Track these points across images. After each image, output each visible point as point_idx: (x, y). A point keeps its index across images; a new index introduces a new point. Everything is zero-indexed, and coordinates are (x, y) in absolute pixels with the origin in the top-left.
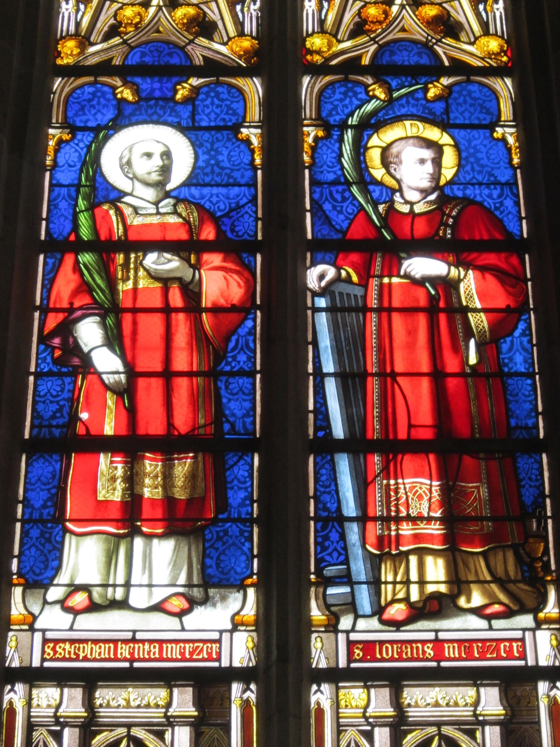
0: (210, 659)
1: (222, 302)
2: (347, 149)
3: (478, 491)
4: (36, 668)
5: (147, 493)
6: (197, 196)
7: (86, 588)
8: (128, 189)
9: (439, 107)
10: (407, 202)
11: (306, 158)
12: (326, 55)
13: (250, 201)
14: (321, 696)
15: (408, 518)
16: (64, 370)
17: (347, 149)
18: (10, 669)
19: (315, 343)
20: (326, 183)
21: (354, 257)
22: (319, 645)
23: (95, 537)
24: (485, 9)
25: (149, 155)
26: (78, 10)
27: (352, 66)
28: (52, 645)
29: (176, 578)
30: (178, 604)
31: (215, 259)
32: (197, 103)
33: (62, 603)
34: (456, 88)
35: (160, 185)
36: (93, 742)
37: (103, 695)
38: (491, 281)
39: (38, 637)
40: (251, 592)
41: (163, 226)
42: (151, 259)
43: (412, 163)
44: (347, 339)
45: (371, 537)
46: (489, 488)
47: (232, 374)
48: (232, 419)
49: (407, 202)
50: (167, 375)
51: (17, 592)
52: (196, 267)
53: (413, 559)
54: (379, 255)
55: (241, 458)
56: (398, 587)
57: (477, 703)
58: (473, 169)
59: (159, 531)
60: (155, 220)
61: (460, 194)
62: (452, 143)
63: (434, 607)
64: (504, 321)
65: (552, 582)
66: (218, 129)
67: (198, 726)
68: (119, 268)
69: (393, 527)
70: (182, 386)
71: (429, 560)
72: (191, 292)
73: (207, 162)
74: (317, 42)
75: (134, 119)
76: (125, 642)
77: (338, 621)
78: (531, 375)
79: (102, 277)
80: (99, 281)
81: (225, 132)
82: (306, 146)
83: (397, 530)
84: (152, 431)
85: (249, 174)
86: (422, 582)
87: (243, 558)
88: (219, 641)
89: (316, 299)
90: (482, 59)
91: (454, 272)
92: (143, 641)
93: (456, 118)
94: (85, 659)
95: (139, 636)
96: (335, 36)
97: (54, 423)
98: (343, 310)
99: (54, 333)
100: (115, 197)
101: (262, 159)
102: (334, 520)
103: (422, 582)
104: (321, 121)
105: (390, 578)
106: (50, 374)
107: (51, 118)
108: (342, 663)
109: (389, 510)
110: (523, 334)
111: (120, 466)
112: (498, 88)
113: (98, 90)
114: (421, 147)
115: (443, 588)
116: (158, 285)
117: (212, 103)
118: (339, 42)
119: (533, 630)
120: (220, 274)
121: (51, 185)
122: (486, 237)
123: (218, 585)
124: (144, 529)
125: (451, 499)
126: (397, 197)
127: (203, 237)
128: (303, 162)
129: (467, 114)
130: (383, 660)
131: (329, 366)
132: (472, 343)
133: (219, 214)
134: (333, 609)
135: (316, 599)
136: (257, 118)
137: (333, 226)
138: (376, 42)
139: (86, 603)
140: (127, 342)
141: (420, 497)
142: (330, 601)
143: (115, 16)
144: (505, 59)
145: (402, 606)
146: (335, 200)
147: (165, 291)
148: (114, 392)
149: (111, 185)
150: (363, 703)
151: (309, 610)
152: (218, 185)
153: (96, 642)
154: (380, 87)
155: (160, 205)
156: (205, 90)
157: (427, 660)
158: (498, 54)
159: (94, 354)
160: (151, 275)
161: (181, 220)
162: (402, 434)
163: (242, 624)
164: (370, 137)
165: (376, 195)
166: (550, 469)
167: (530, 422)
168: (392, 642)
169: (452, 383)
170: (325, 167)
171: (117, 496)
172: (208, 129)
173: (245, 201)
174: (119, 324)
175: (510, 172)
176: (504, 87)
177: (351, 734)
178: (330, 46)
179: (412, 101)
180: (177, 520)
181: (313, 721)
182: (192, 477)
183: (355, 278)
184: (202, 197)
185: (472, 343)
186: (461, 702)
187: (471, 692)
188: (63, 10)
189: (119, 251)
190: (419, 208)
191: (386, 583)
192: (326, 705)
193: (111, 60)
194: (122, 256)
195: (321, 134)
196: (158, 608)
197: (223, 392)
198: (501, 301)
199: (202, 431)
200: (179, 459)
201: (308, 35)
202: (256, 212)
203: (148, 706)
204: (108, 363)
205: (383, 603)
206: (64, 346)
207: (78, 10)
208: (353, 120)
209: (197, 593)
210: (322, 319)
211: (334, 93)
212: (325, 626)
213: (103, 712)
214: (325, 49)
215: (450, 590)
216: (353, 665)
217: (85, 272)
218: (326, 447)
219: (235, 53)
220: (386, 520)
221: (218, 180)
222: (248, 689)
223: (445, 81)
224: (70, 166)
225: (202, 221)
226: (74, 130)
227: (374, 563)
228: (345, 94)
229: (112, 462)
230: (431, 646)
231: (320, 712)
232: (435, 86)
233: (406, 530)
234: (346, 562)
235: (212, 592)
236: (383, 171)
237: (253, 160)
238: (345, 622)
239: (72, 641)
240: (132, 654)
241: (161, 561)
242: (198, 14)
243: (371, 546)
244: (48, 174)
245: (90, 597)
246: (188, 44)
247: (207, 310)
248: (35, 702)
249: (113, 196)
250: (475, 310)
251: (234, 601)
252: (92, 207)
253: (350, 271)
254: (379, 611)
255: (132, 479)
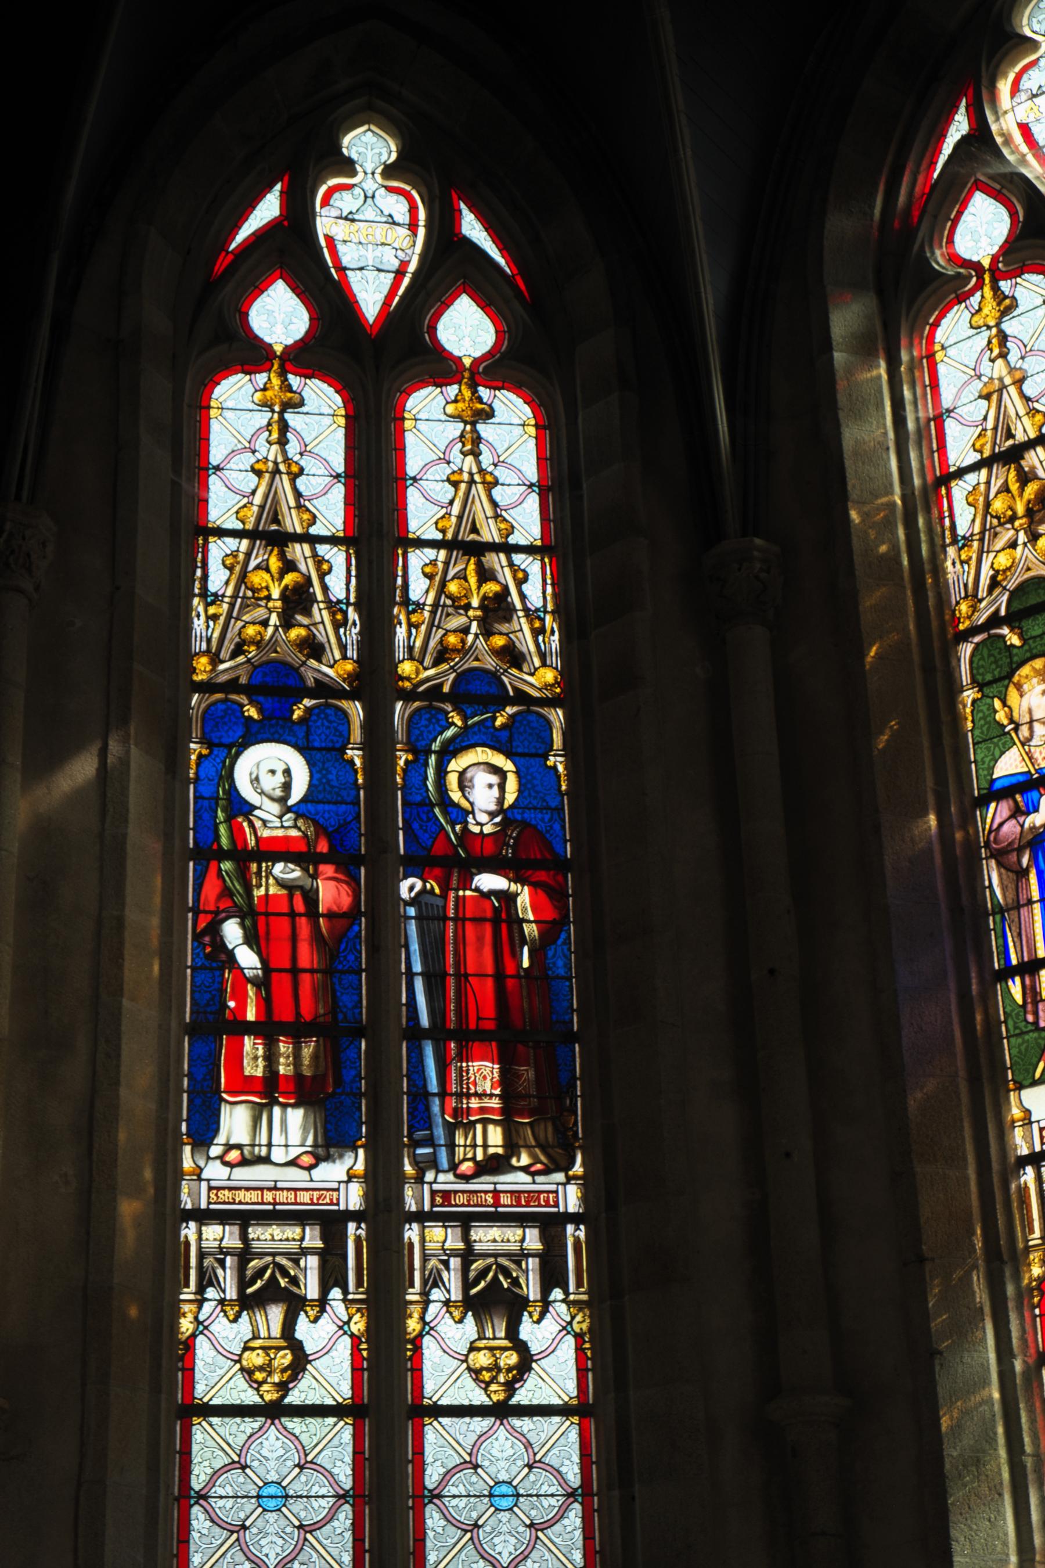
0: (332, 1204)
1: (335, 908)
2: (431, 772)
3: (527, 1073)
4: (204, 1210)
5: (282, 1070)
6: (313, 811)
7: (239, 1147)
8: (258, 804)
9: (505, 735)
10: (478, 824)
11: (399, 780)
12: (414, 682)
13: (355, 819)
14: (412, 1233)
15: (476, 1094)
16: (214, 965)
17: (431, 772)
18: (184, 1210)
19: (407, 947)
20: (415, 804)
21: (437, 871)
22: (410, 1193)
23: (243, 1106)
24: (544, 641)
25: (273, 772)
26: (208, 627)
27: (435, 692)
28: (215, 1192)
29: (305, 1139)
30: (307, 1160)
31: (328, 870)
32: (310, 723)
33: (221, 1158)
34: (519, 718)
35: (282, 800)
36: (473, 1267)
37: (254, 1232)
38: (541, 894)
39: (204, 1184)
40: (361, 1152)
41: (286, 839)
42: (278, 868)
43: (482, 786)
44: (431, 943)
45: (448, 1109)
46: (535, 1071)
47: (342, 972)
48: (344, 1010)
49: (478, 824)
50: (295, 971)
51: (187, 1149)
52: (314, 877)
53: (479, 1127)
54: (456, 870)
55: (352, 1042)
56: (468, 1149)
57: (523, 1240)
58: (530, 795)
59: (292, 1101)
60: (280, 833)
61: (519, 817)
62: (514, 769)
63: (494, 1165)
64: (550, 930)
65: (580, 1147)
66: (328, 750)
67: (323, 1255)
68: (254, 876)
69: (465, 1101)
70: (306, 979)
71: (491, 1128)
72: (311, 898)
73: (320, 780)
74: (407, 668)
75: (260, 736)
76: (270, 1189)
77: (424, 1175)
78: (570, 979)
79: (240, 884)
80: (238, 887)
81: (333, 753)
82: (398, 768)
83: (468, 1103)
84: (285, 1019)
85: (353, 792)
86: (485, 1146)
87: (355, 1124)
88: (337, 1190)
89: (408, 908)
90: (540, 689)
91: (513, 887)
92: (282, 1189)
93: (518, 746)
94: (240, 1203)
95: (280, 1185)
96: (422, 663)
97: (209, 1010)
98: (428, 918)
99: (204, 932)
100: (247, 809)
101: (364, 779)
102: (420, 1096)
103: (485, 1146)
104: (411, 749)
105: (462, 1143)
106: (203, 968)
107: (191, 733)
108: (427, 1208)
109: (462, 1088)
110: (564, 943)
111: (260, 1047)
112: (552, 719)
113: (228, 708)
114: (490, 773)
115: (500, 1151)
116: (284, 892)
117: (323, 725)
118: (426, 669)
119: (564, 1185)
120: (333, 883)
121: (195, 798)
122: (539, 857)
123: (336, 1145)
124: (281, 1100)
125: (507, 1080)
126: (470, 819)
127: (319, 850)
128: (397, 783)
129: (526, 743)
130: (456, 1206)
131: (417, 967)
132: (526, 949)
133: (331, 829)
134: (421, 1165)
135: (409, 1157)
136: (359, 740)
137: (420, 843)
138: (455, 671)
139: (240, 1158)
140: (263, 942)
141: (485, 1078)
142: (419, 1159)
143: (240, 634)
144: (558, 690)
145: (470, 1164)
146: (422, 820)
147: (291, 896)
148: (254, 984)
149: (244, 799)
150: (442, 1239)
151: (403, 1165)
152: (329, 803)
153: (247, 1189)
154: (458, 714)
155: (284, 819)
156: (317, 711)
157: (488, 1206)
158: (552, 685)
159: (236, 951)
160: (280, 883)
161: (300, 834)
162: (472, 1026)
163: (355, 1177)
164: (449, 762)
165: (454, 816)
166: (580, 1057)
167: (567, 1017)
168: (463, 1192)
169: (510, 983)
170: (414, 789)
171: (259, 1073)
172: (320, 749)
173: (350, 818)
174: (255, 925)
175: (559, 799)
176: (557, 716)
177: (433, 1262)
178: (417, 673)
179: (483, 730)
180: (304, 1092)
181: (406, 1252)
182: (315, 1057)
183: (437, 891)
184: (317, 813)
185: (526, 949)
186: (512, 1239)
187: (520, 1232)
188: (195, 626)
189: (253, 861)
190: (488, 829)
191: (459, 1146)
192: (416, 1240)
193: (238, 678)
194: (255, 865)
195: (410, 757)
196: (293, 1163)
197: (337, 987)
198: (550, 914)
199: (321, 1019)
200: (305, 1042)
201: (400, 662)
202: (360, 828)
203: (287, 1240)
204: (248, 959)
205: (457, 1161)
206: (213, 944)
207: (208, 627)
208: (436, 746)
209: (321, 1151)
210: (412, 927)
211: (421, 719)
212: (415, 1178)
213: (255, 1244)
214: (413, 676)
215: (505, 1151)
216: (435, 1209)
217: (227, 878)
218: (414, 1034)
219: (340, 676)
220: (460, 1095)
221: (329, 797)
222: (358, 1228)
223: (510, 710)
224: (210, 780)
225: (317, 835)
226: (210, 745)
227: (451, 1130)
228: (429, 720)
229: (255, 1044)
230: (491, 1195)
231: (411, 1245)
232: (502, 715)
233: (474, 1103)
234: (430, 1128)
235: (332, 1150)
236: (460, 794)
237: (357, 780)
238: (429, 1176)
239: (230, 1189)
240: (274, 1199)
241: (292, 1127)
242: (309, 635)
243: (450, 1116)
244: (192, 786)
245: (242, 1154)
246: (301, 666)
247: (323, 915)
248: (204, 1237)
249: (246, 809)
250: (529, 921)
251: (348, 1160)
252: (230, 819)
253: (434, 884)
254: (453, 1167)
255: (271, 1058)
